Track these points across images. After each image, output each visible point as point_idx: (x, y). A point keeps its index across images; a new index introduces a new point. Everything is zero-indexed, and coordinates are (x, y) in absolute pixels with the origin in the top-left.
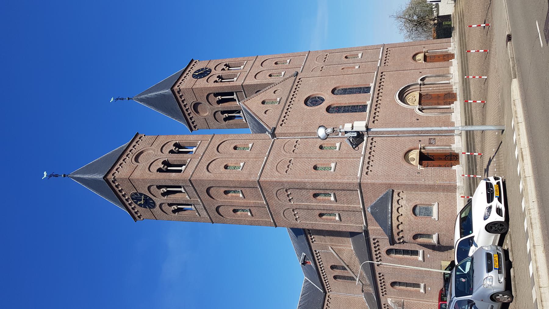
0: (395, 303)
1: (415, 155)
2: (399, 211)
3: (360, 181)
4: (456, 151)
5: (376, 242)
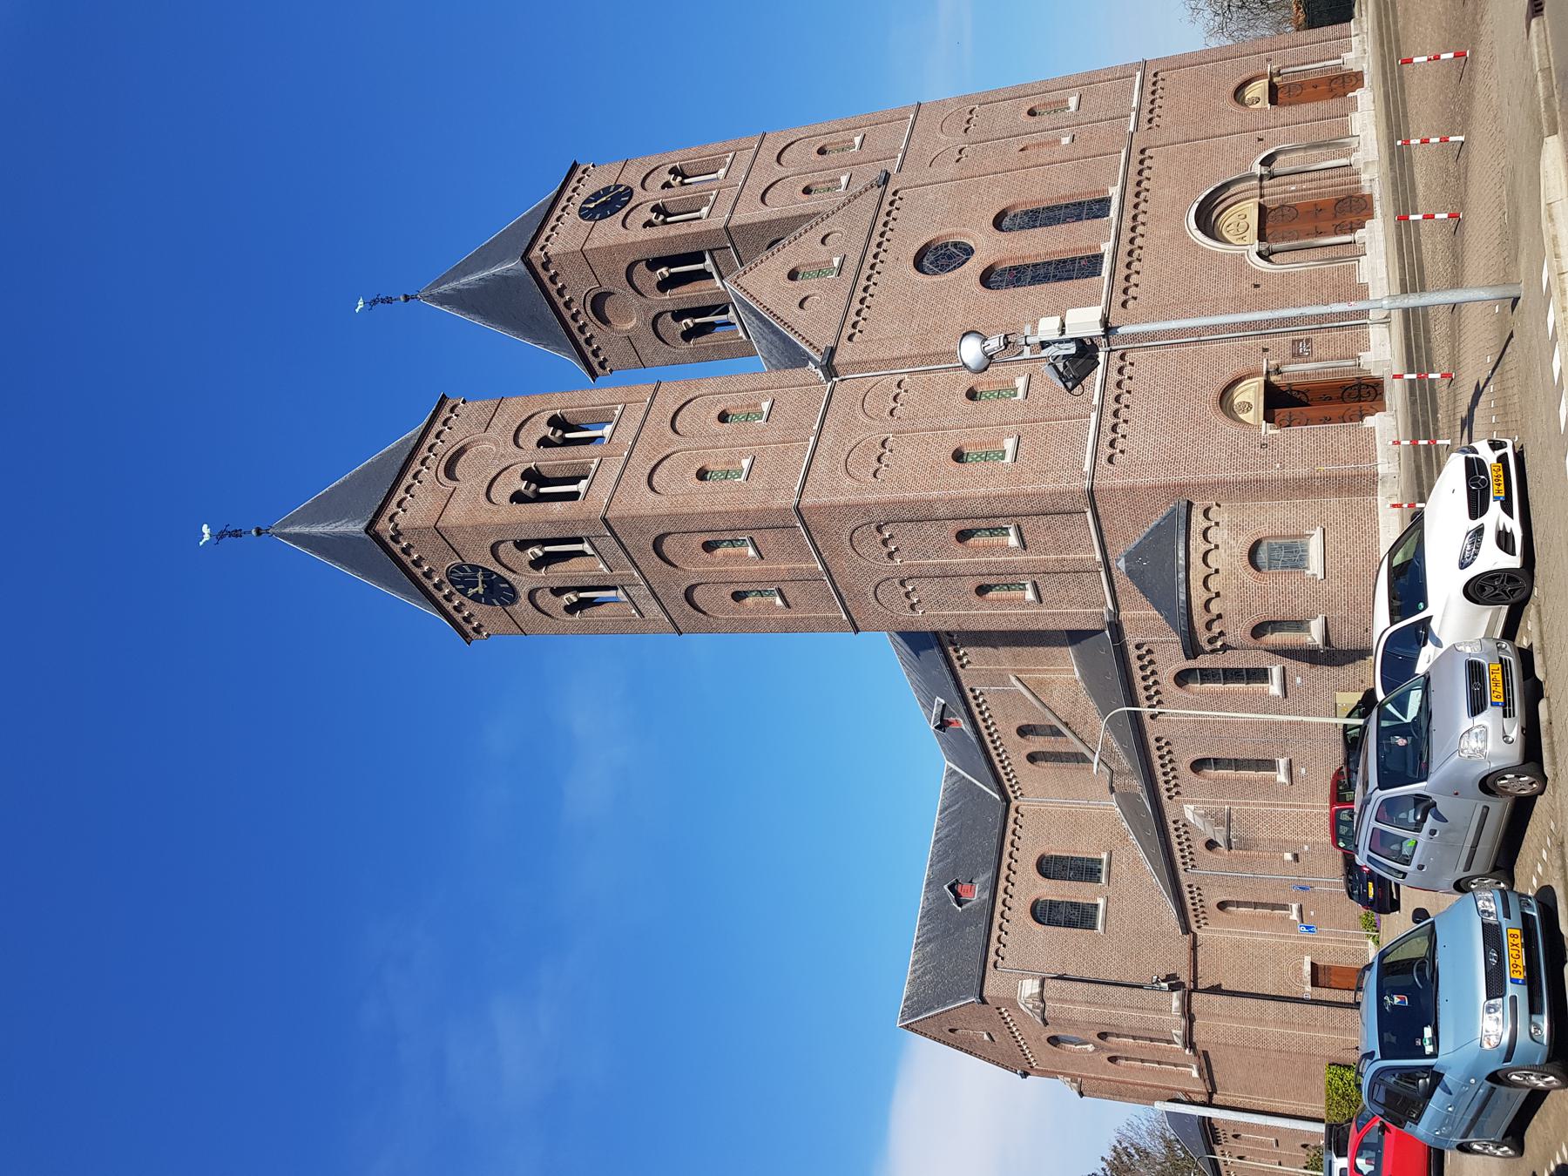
0: (1206, 815)
3: (1092, 483)
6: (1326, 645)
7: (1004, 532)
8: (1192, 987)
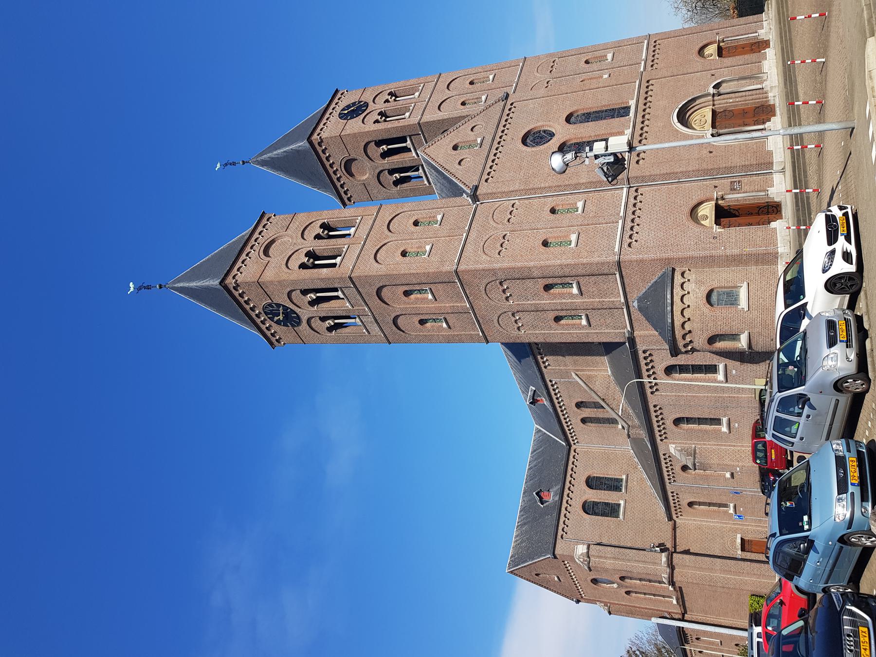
0: (682, 450)
1: (708, 210)
2: (684, 300)
3: (619, 259)
4: (776, 198)
5: (648, 355)
7: (570, 286)
8: (673, 551)
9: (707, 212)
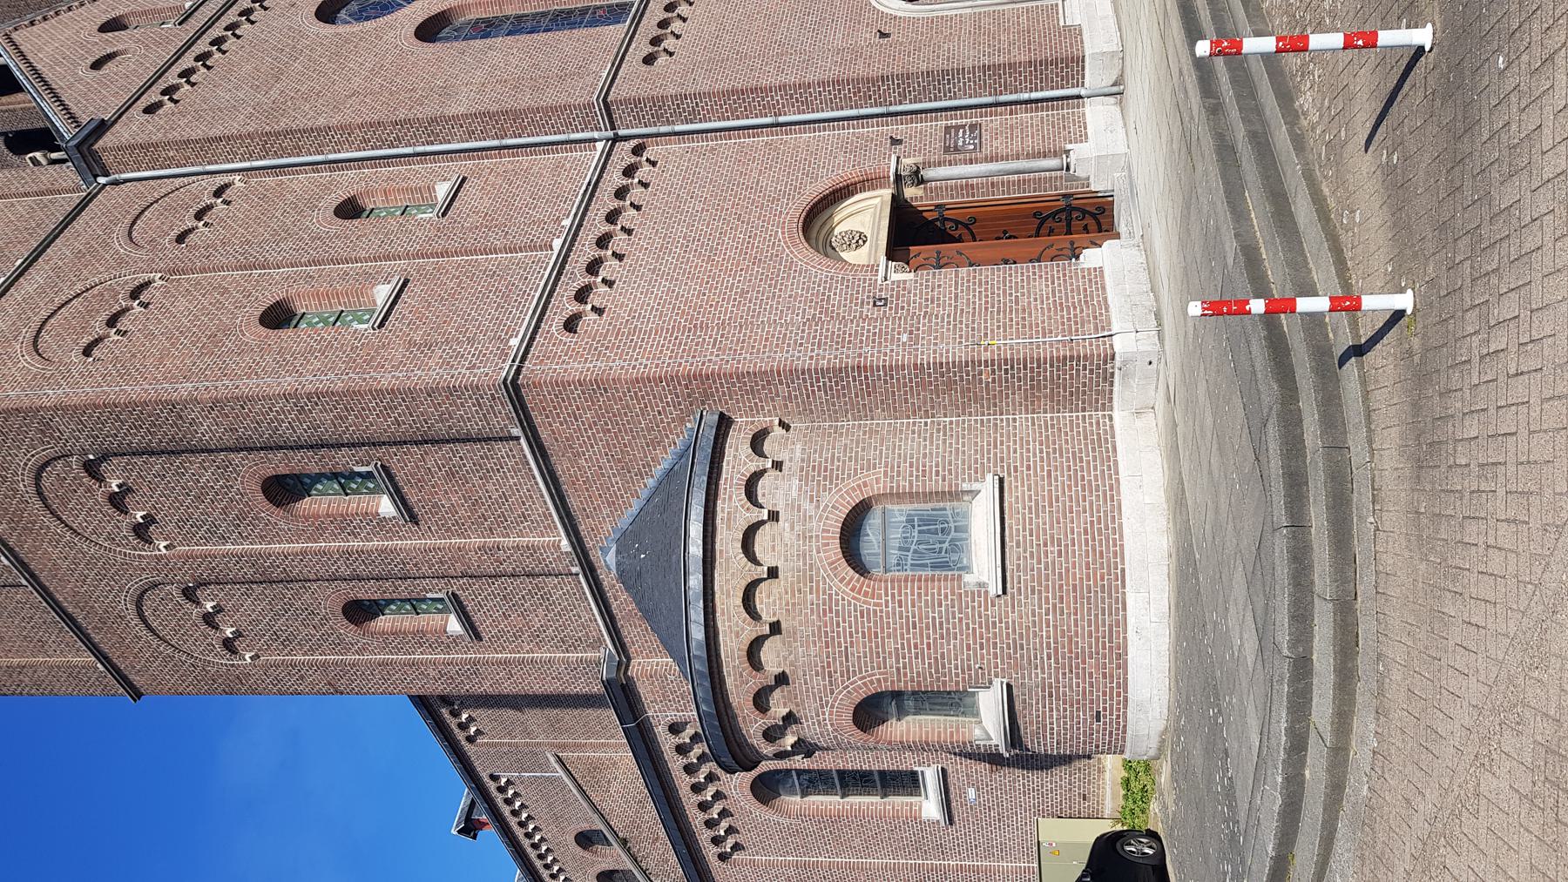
2: (757, 548)
6: (1013, 746)
9: (863, 225)
